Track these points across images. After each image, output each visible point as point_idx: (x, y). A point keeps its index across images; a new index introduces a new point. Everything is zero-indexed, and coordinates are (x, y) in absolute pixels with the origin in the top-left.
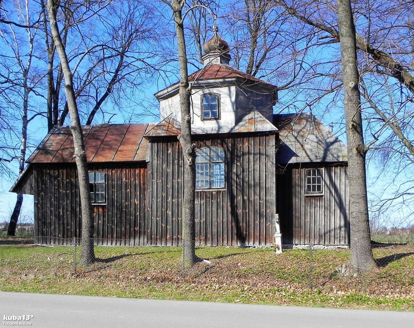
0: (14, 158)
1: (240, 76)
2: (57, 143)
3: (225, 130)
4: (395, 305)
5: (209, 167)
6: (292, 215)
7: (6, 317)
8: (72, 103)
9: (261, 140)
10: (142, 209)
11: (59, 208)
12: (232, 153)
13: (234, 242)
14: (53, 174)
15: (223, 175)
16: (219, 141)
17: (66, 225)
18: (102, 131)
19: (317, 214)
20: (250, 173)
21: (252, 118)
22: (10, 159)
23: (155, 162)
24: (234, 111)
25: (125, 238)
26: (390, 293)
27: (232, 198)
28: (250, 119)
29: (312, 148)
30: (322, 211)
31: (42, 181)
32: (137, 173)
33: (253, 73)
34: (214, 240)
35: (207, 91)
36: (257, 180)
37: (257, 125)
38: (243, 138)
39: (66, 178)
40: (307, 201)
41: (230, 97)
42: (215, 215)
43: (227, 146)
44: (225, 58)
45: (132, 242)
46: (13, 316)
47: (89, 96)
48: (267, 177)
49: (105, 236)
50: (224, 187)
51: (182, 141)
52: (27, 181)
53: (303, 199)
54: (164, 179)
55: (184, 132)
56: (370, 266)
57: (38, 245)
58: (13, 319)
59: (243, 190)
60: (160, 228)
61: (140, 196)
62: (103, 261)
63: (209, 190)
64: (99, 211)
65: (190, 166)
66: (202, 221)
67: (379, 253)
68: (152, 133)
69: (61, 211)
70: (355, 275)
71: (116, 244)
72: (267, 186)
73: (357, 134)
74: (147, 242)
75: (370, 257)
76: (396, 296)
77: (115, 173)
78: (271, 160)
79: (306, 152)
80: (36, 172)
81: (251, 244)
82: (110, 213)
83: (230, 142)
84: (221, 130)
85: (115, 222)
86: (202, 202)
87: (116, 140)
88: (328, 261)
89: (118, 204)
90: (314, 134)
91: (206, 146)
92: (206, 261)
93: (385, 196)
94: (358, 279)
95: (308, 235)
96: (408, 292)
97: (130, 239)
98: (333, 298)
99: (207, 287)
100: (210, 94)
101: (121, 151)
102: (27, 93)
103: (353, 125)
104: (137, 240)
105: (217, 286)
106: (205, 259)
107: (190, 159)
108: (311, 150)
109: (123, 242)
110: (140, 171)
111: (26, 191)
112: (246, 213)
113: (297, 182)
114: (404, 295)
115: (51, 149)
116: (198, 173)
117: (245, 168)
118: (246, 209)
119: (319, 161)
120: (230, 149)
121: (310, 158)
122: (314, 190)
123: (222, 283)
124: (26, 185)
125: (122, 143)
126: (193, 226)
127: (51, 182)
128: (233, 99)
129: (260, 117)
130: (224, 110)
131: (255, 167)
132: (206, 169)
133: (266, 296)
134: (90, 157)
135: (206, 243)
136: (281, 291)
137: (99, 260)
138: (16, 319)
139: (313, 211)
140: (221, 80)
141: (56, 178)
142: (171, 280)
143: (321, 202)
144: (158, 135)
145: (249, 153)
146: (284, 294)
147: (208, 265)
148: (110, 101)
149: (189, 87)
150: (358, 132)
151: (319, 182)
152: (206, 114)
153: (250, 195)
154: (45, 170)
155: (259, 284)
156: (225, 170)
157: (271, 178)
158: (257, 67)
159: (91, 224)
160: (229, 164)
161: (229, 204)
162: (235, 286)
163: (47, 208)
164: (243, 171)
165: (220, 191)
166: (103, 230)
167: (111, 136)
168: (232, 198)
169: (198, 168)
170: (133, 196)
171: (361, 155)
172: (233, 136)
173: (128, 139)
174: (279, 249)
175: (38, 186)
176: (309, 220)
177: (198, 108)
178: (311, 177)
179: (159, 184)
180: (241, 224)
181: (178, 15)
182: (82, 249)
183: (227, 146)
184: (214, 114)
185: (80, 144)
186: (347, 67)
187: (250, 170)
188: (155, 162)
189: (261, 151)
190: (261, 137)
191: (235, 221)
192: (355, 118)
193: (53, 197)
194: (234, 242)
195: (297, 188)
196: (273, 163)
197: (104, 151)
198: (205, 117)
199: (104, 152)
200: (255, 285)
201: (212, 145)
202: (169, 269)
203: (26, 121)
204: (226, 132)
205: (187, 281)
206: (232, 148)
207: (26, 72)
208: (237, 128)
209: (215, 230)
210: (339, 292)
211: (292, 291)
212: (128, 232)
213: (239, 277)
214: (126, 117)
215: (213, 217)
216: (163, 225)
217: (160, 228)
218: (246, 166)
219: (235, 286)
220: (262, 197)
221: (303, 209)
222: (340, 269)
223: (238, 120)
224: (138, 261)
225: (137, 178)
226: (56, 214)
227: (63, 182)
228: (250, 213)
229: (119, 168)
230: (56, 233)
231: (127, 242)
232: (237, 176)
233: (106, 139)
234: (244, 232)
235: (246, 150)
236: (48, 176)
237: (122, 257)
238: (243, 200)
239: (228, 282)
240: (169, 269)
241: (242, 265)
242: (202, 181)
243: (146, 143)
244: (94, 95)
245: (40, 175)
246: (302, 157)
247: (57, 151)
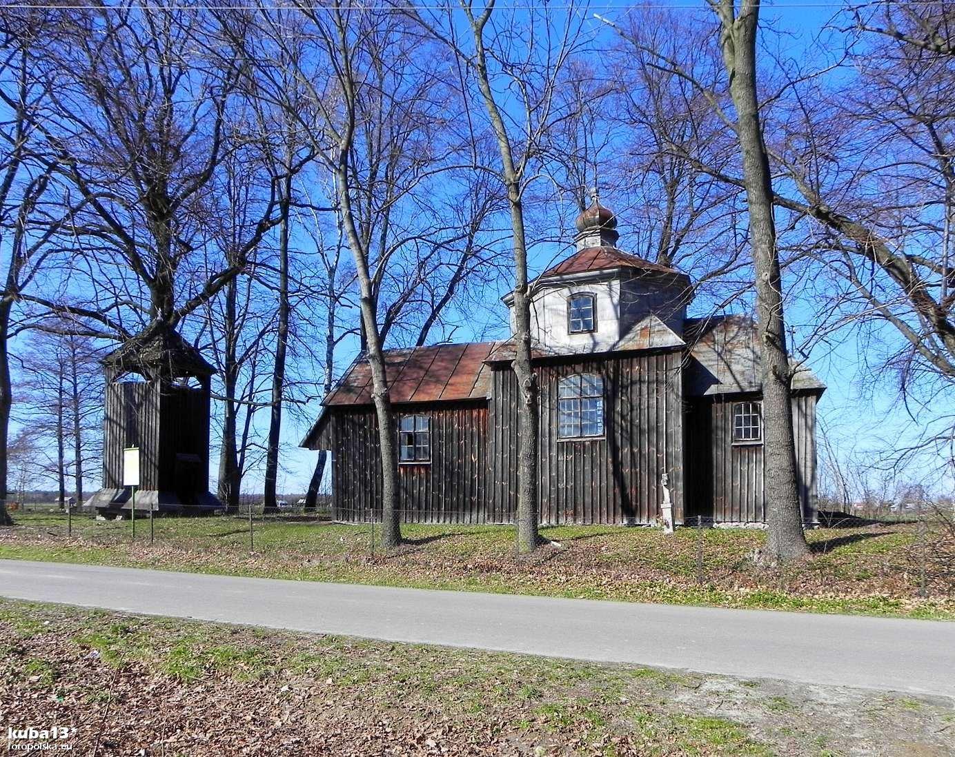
0: (310, 398)
1: (627, 264)
2: (364, 376)
3: (603, 348)
4: (824, 608)
5: (579, 404)
6: (712, 477)
8: (371, 321)
9: (660, 361)
10: (482, 469)
11: (365, 470)
12: (615, 382)
13: (618, 519)
14: (357, 421)
15: (600, 415)
16: (595, 365)
18: (428, 356)
19: (752, 474)
20: (642, 412)
21: (646, 327)
22: (303, 399)
23: (500, 398)
24: (617, 319)
25: (478, 512)
26: (820, 592)
27: (615, 451)
28: (642, 329)
29: (744, 369)
30: (760, 469)
31: (343, 430)
32: (474, 416)
33: (670, 250)
34: (586, 514)
35: (575, 290)
36: (653, 423)
37: (653, 338)
38: (632, 358)
40: (735, 452)
41: (611, 297)
42: (588, 477)
43: (607, 372)
44: (609, 234)
45: (467, 518)
47: (422, 301)
48: (669, 416)
49: (425, 509)
50: (602, 434)
51: (517, 370)
53: (729, 449)
54: (512, 425)
55: (522, 356)
56: (798, 552)
57: (336, 521)
59: (631, 438)
60: (506, 497)
62: (411, 542)
63: (580, 440)
64: (420, 473)
65: (528, 405)
66: (569, 487)
67: (819, 534)
68: (494, 357)
69: (368, 473)
70: (773, 564)
71: (444, 522)
72: (669, 431)
73: (776, 350)
74: (488, 519)
75: (799, 539)
76: (829, 595)
77: (443, 417)
79: (734, 376)
81: (644, 521)
82: (436, 476)
83: (611, 365)
84: (597, 349)
86: (570, 457)
87: (446, 368)
88: (740, 544)
89: (448, 463)
90: (749, 348)
91: (575, 372)
92: (555, 543)
93: (902, 444)
94: (776, 571)
95: (738, 507)
96: (849, 590)
98: (729, 597)
99: (549, 580)
100: (581, 294)
101: (451, 385)
102: (333, 304)
103: (768, 337)
104: (474, 516)
105: (564, 578)
106: (555, 541)
107: (529, 396)
108: (743, 373)
109: (454, 518)
110: (479, 413)
112: (636, 473)
113: (719, 424)
114: (842, 595)
115: (356, 384)
116: (564, 414)
117: (634, 404)
118: (636, 468)
119: (754, 389)
120: (612, 375)
121: (740, 387)
122: (747, 435)
123: (571, 575)
125: (454, 373)
126: (534, 493)
128: (616, 299)
129: (659, 325)
130: (602, 317)
131: (651, 402)
132: (575, 407)
133: (632, 592)
134: (408, 395)
135: (575, 520)
136: (655, 586)
137: (407, 541)
139: (746, 468)
140: (597, 272)
141: (361, 426)
142: (500, 569)
143: (758, 455)
144: (504, 359)
145: (641, 382)
146: (658, 591)
147: (556, 549)
148: (453, 306)
149: (528, 293)
150: (777, 348)
151: (755, 423)
152: (576, 325)
153: (642, 446)
155: (625, 576)
156: (604, 409)
157: (676, 420)
158: (678, 242)
159: (395, 490)
160: (610, 397)
161: (610, 460)
162: (590, 578)
164: (632, 410)
165: (597, 441)
166: (426, 500)
167: (439, 363)
168: (615, 451)
169: (563, 406)
170: (469, 450)
171: (782, 382)
172: (615, 356)
173: (463, 367)
174: (668, 527)
175: (337, 438)
176: (739, 482)
177: (563, 316)
178: (743, 415)
179: (505, 432)
180: (628, 491)
181: (513, 190)
182: (381, 526)
183: (607, 372)
184: (587, 324)
185: (381, 378)
186: (759, 249)
187: (642, 407)
188: (500, 398)
189: (660, 378)
190: (659, 357)
191: (619, 486)
192: (773, 327)
193: (357, 454)
194: (618, 519)
195: (719, 433)
196: (677, 395)
197: (429, 385)
198: (573, 329)
199: (427, 387)
200: (618, 577)
201: (583, 371)
202: (501, 554)
203: (331, 342)
204: (605, 351)
205: (522, 571)
206: (614, 373)
207: (332, 271)
208: (621, 343)
209: (588, 500)
210: (741, 589)
211: (670, 586)
212: (462, 503)
213: (599, 565)
214: (476, 330)
215: (586, 480)
216: (512, 493)
217: (506, 497)
218: (636, 402)
219: (590, 578)
220: (661, 448)
221: (729, 466)
222: (751, 556)
223: (624, 331)
224: (461, 544)
225: (474, 423)
227: (371, 432)
228: (643, 473)
229: (449, 410)
231: (460, 517)
232: (623, 417)
233: (433, 367)
234: (634, 503)
235: (636, 377)
236: (351, 424)
237: (440, 537)
238: (632, 453)
239: (580, 573)
240: (501, 554)
241: (607, 549)
242: (569, 426)
243: (487, 371)
244: (429, 299)
245: (341, 421)
246: (727, 385)
247: (363, 388)
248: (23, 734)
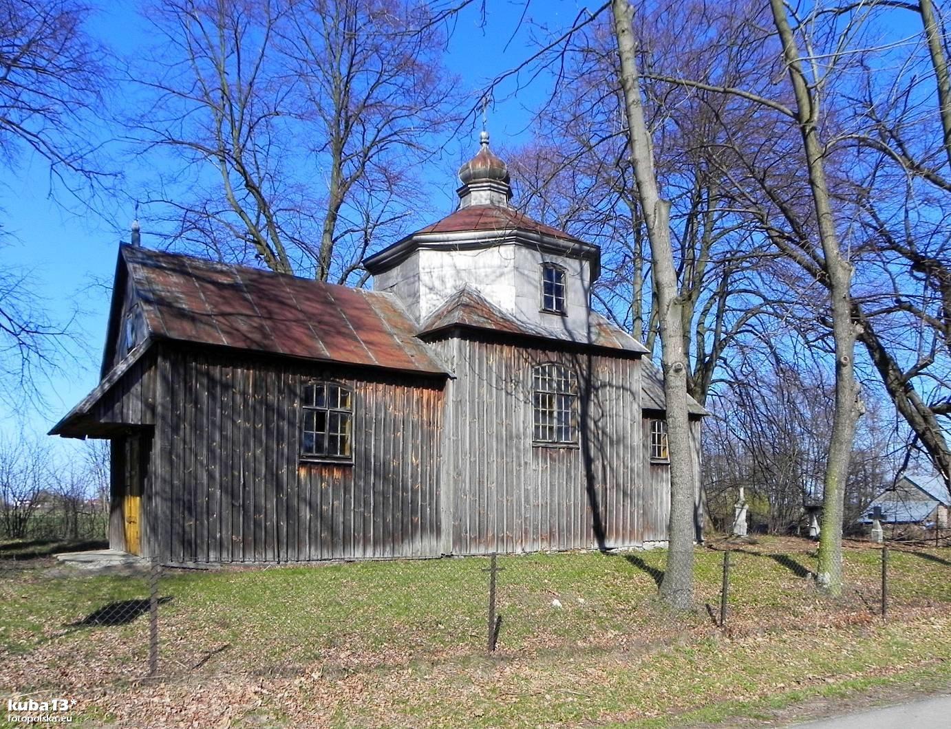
7: (15, 704)
14: (218, 376)
17: (252, 509)
31: (188, 389)
39: (255, 391)
41: (582, 280)
46: (31, 701)
52: (133, 385)
58: (31, 708)
61: (422, 448)
80: (168, 365)
85: (372, 504)
100: (554, 265)
109: (388, 549)
111: (128, 414)
120: (585, 372)
124: (128, 398)
138: (36, 709)
154: (196, 361)
163: (199, 466)
226: (224, 483)
230: (224, 532)
248: (23, 706)
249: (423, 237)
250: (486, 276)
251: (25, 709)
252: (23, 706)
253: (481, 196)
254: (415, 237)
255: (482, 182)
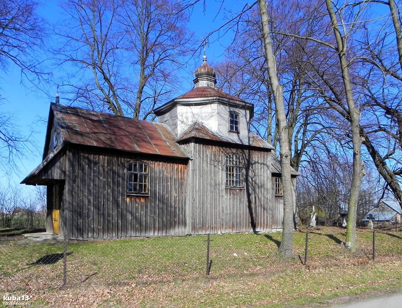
7: (6, 297)
14: (92, 159)
17: (107, 215)
39: (108, 165)
41: (246, 118)
46: (13, 296)
52: (56, 163)
58: (13, 299)
61: (178, 189)
78: (77, 183)
80: (71, 154)
85: (157, 213)
97: (162, 231)
100: (234, 112)
109: (164, 232)
111: (54, 175)
124: (54, 168)
127: (90, 167)
138: (15, 299)
154: (83, 153)
163: (84, 197)
226: (95, 204)
230: (95, 225)
248: (10, 298)
249: (179, 100)
250: (205, 116)
251: (11, 299)
252: (10, 298)
253: (203, 83)
254: (175, 100)
255: (204, 77)
